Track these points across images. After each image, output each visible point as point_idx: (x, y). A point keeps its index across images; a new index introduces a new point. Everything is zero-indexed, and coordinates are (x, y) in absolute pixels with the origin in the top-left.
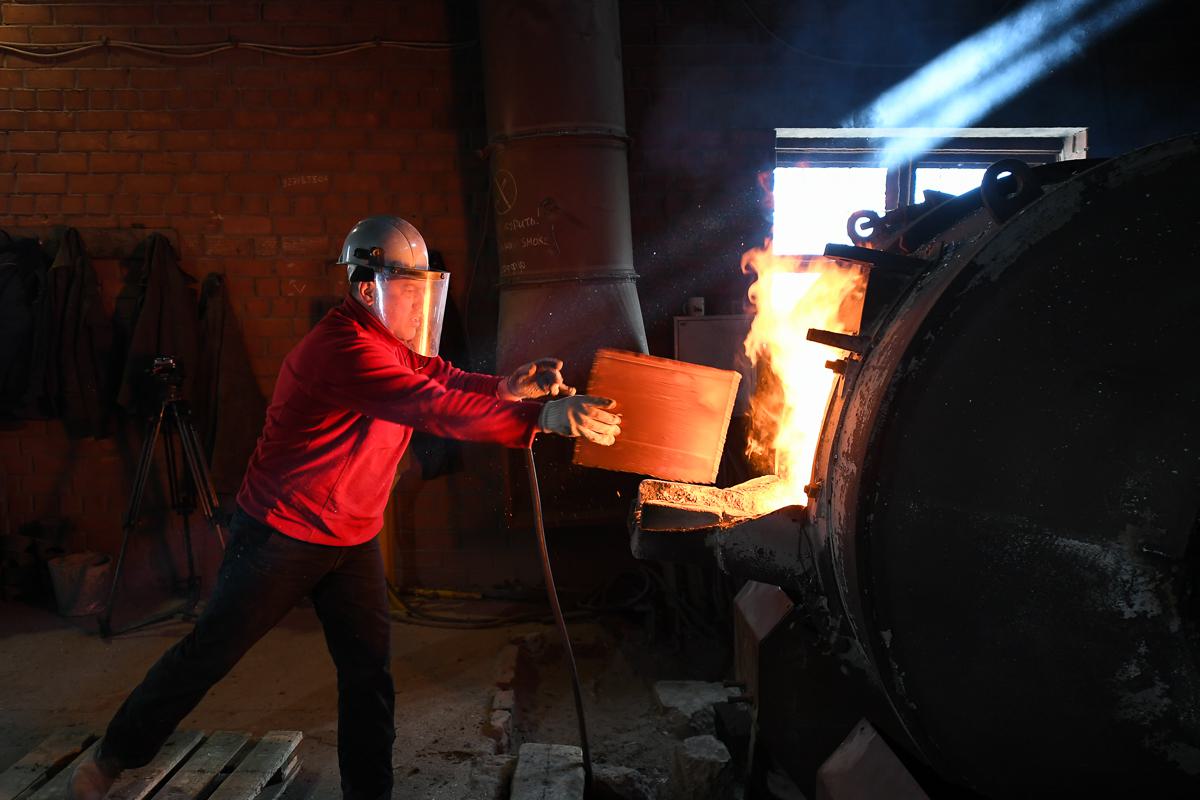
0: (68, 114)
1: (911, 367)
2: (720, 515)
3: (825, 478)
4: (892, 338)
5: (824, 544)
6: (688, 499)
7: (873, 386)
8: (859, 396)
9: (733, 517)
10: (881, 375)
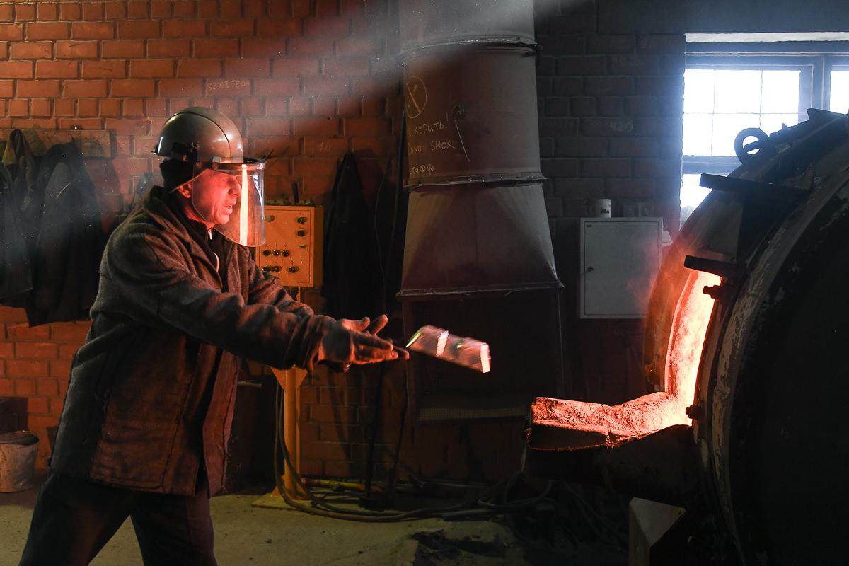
0: (19, 25)
1: (779, 297)
2: (607, 434)
3: (706, 400)
4: (765, 266)
5: (706, 465)
6: (579, 417)
7: (748, 312)
8: (734, 323)
9: (619, 436)
10: (754, 302)
